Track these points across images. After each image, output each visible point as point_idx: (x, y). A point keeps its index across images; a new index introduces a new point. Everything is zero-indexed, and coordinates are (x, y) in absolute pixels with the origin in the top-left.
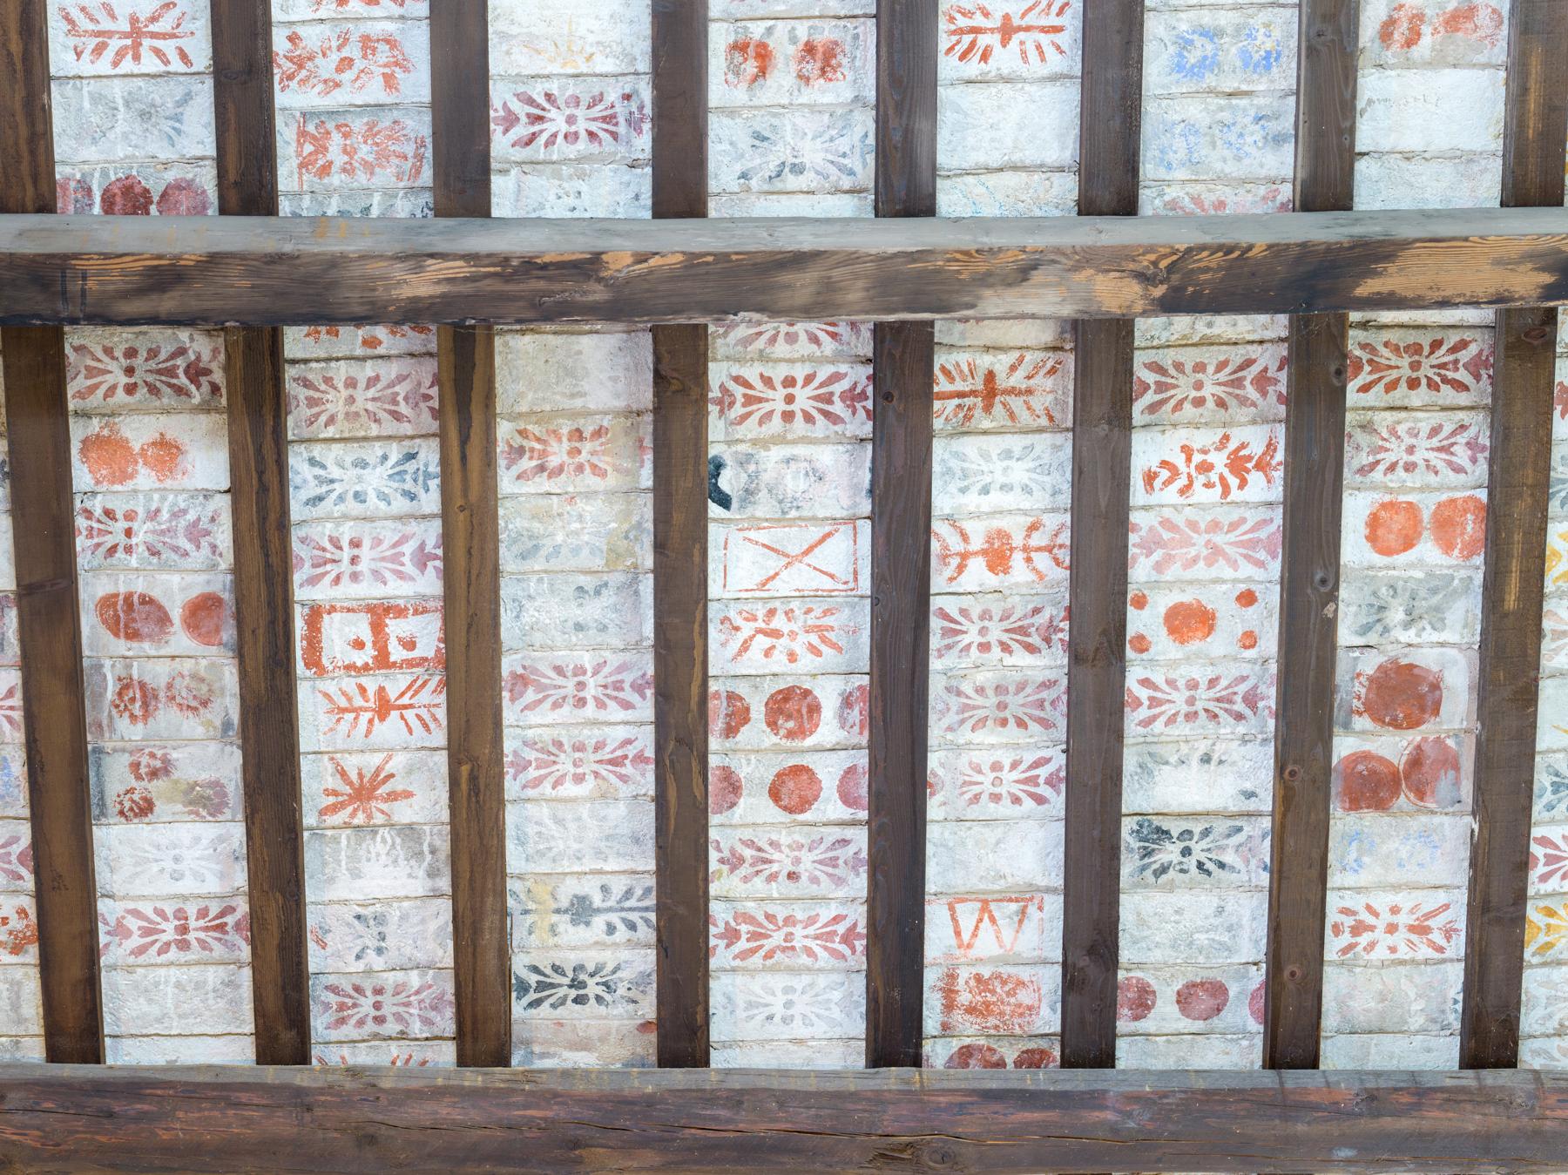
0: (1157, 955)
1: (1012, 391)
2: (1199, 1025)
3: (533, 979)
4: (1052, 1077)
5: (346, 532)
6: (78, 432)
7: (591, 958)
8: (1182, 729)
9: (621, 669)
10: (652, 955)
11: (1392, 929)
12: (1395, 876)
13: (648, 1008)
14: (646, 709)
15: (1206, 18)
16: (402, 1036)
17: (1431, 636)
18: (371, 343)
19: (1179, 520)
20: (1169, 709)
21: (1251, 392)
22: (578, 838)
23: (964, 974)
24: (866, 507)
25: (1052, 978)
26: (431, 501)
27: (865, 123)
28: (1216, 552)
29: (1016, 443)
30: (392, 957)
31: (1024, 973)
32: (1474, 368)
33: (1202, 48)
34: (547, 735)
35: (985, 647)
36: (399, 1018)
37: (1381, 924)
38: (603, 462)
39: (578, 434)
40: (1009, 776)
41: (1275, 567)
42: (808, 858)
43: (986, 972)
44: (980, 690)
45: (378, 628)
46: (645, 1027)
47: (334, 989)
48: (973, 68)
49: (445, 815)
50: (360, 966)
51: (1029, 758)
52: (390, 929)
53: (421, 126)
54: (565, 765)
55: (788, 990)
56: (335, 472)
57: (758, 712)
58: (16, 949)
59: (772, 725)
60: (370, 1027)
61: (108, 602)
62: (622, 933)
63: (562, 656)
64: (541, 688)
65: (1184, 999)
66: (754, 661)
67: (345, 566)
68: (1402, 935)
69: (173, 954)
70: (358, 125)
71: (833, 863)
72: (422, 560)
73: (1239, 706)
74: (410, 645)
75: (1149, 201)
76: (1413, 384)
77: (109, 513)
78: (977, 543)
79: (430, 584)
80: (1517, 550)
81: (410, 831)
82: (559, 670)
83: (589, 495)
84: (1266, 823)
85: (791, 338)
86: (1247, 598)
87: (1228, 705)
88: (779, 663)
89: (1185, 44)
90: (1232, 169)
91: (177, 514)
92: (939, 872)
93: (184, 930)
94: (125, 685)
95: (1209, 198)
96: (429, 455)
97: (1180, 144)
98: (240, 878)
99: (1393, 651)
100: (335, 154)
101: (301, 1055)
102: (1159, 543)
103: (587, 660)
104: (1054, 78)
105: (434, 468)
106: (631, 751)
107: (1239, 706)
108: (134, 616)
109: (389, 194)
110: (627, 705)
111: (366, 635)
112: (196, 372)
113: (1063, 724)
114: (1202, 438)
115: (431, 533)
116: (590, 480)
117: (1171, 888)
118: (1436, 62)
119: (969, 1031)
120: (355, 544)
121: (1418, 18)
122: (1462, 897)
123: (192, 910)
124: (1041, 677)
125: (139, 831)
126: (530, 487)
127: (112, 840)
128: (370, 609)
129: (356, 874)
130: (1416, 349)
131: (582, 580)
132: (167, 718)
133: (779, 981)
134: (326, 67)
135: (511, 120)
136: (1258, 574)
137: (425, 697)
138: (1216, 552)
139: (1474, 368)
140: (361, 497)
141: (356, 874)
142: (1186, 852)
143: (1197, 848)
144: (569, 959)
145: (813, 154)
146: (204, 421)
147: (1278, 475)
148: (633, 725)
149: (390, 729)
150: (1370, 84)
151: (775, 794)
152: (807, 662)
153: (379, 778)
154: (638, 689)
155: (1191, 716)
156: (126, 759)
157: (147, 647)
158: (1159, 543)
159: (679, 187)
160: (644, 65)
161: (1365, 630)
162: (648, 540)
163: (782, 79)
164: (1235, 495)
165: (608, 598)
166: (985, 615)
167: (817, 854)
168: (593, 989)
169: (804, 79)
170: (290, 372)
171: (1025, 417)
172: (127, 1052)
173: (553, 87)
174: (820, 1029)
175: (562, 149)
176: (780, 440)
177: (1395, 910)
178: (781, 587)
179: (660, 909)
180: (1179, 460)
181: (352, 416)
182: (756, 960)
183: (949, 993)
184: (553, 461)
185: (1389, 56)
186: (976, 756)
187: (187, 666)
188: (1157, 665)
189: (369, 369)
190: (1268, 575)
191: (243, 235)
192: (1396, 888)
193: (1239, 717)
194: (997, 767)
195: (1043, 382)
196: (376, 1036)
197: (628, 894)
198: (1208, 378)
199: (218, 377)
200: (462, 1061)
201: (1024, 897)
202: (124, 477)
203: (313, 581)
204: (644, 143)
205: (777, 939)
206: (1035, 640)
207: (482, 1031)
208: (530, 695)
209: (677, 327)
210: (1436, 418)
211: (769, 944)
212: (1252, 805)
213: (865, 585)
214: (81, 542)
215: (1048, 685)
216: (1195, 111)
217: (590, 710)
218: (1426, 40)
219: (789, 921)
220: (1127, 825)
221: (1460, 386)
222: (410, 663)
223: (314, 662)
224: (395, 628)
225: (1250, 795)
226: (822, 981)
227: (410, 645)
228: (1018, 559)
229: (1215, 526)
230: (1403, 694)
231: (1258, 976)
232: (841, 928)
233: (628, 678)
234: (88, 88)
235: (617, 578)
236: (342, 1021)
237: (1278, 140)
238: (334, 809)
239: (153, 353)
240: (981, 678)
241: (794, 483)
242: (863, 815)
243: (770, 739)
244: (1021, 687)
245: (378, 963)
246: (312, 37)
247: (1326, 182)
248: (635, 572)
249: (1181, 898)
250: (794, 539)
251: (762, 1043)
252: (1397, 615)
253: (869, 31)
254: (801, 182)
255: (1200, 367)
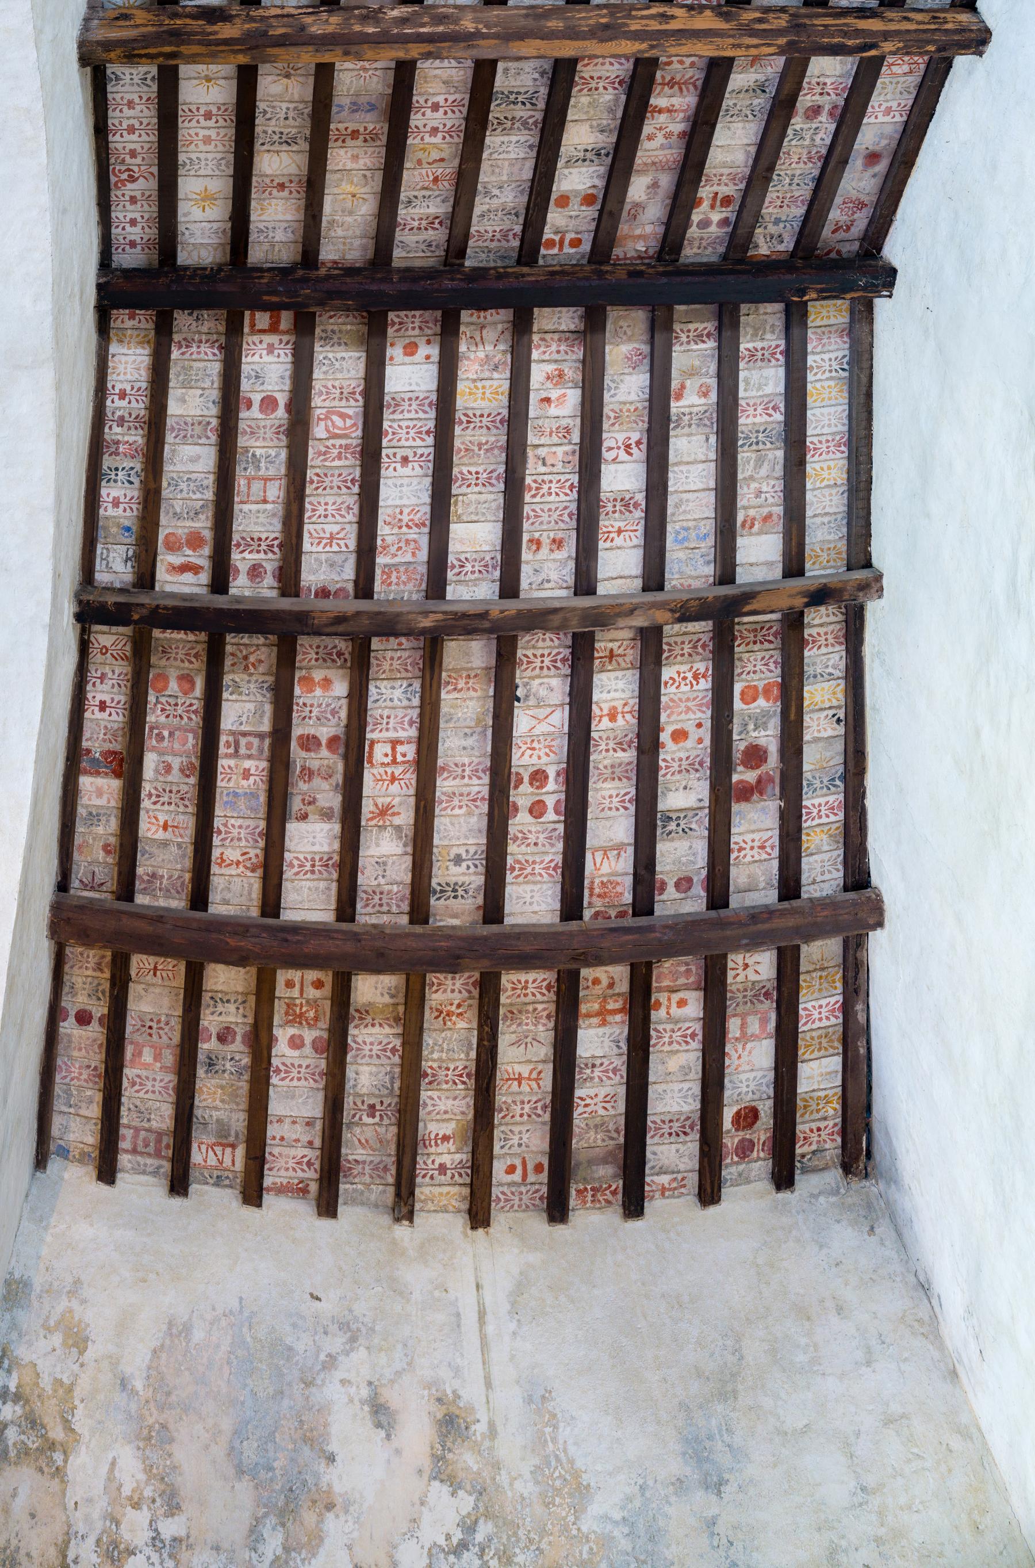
0: (668, 868)
1: (619, 655)
2: (683, 895)
3: (439, 888)
4: (630, 921)
5: (386, 713)
6: (298, 674)
7: (461, 879)
8: (677, 777)
9: (479, 764)
10: (483, 878)
11: (752, 848)
12: (753, 827)
13: (480, 900)
14: (486, 780)
15: (685, 524)
16: (389, 912)
17: (763, 733)
18: (400, 644)
19: (676, 698)
20: (672, 770)
21: (700, 650)
22: (459, 829)
23: (597, 881)
24: (567, 700)
25: (629, 880)
26: (416, 701)
27: (572, 564)
28: (688, 709)
29: (620, 674)
30: (388, 879)
31: (619, 879)
32: (775, 635)
33: (683, 534)
34: (450, 790)
35: (607, 751)
36: (388, 904)
37: (748, 847)
38: (477, 687)
39: (468, 677)
40: (615, 800)
41: (709, 713)
42: (542, 836)
43: (605, 880)
44: (606, 767)
45: (394, 749)
46: (479, 908)
47: (365, 892)
48: (608, 544)
49: (412, 822)
50: (376, 883)
51: (622, 792)
52: (388, 868)
53: (423, 569)
54: (456, 802)
55: (532, 891)
56: (384, 691)
57: (526, 779)
58: (253, 871)
59: (531, 784)
60: (377, 908)
61: (301, 737)
62: (472, 869)
63: (458, 760)
64: (449, 772)
65: (677, 885)
66: (526, 760)
67: (384, 726)
68: (756, 850)
69: (309, 875)
70: (402, 569)
71: (550, 838)
72: (411, 723)
73: (697, 766)
74: (404, 755)
75: (667, 586)
76: (755, 643)
77: (305, 704)
78: (606, 712)
79: (413, 732)
80: (794, 698)
81: (398, 828)
82: (456, 765)
83: (471, 699)
84: (707, 811)
85: (544, 640)
86: (699, 725)
87: (693, 766)
88: (535, 760)
89: (678, 533)
90: (693, 573)
91: (328, 705)
92: (591, 840)
93: (313, 866)
94: (303, 768)
95: (686, 584)
96: (417, 685)
97: (676, 566)
98: (336, 845)
99: (750, 740)
100: (394, 579)
101: (352, 919)
102: (669, 707)
103: (466, 761)
104: (635, 547)
105: (418, 689)
106: (480, 796)
107: (697, 766)
108: (310, 743)
109: (411, 593)
110: (479, 778)
111: (389, 752)
112: (340, 654)
113: (635, 778)
114: (684, 668)
115: (415, 713)
116: (472, 693)
117: (672, 840)
118: (760, 533)
119: (599, 904)
120: (388, 717)
121: (754, 519)
122: (777, 832)
123: (317, 858)
124: (627, 761)
125: (302, 826)
126: (451, 696)
127: (293, 828)
128: (392, 742)
129: (378, 845)
130: (756, 630)
131: (467, 730)
132: (317, 781)
133: (529, 887)
134: (393, 550)
135: (453, 567)
136: (703, 716)
137: (408, 775)
138: (688, 709)
139: (775, 635)
140: (393, 700)
141: (378, 845)
142: (678, 825)
143: (682, 823)
144: (452, 880)
145: (554, 576)
146: (341, 672)
147: (710, 679)
148: (480, 786)
149: (395, 788)
150: (740, 542)
151: (531, 812)
152: (545, 759)
153: (389, 807)
154: (484, 771)
155: (680, 772)
156: (300, 797)
157: (313, 755)
158: (669, 707)
159: (509, 588)
160: (499, 548)
161: (740, 733)
162: (491, 715)
163: (544, 551)
164: (695, 687)
165: (475, 737)
166: (608, 738)
167: (545, 835)
168: (460, 892)
169: (552, 550)
170: (372, 654)
171: (623, 664)
172: (288, 916)
173: (468, 556)
174: (544, 907)
175: (470, 576)
176: (539, 677)
177: (753, 841)
178: (536, 731)
179: (487, 859)
180: (676, 676)
181: (391, 671)
182: (521, 879)
183: (591, 889)
184: (459, 687)
185: (744, 532)
186: (604, 793)
187: (326, 762)
188: (670, 752)
189: (399, 654)
190: (706, 716)
191: (363, 605)
192: (753, 832)
193: (697, 770)
194: (611, 797)
195: (630, 652)
196: (379, 912)
197: (476, 853)
198: (686, 646)
199: (347, 656)
200: (411, 922)
201: (620, 847)
202: (312, 691)
203: (373, 731)
204: (497, 574)
205: (529, 870)
206: (625, 746)
207: (419, 912)
208: (445, 775)
209: (504, 635)
210: (763, 654)
211: (525, 872)
212: (701, 804)
213: (566, 729)
214: (294, 714)
215: (629, 764)
216: (681, 555)
217: (466, 780)
218: (756, 526)
219: (534, 862)
220: (659, 816)
221: (770, 642)
222: (404, 762)
223: (370, 762)
224: (400, 749)
225: (701, 800)
226: (545, 886)
227: (404, 755)
228: (620, 716)
229: (688, 700)
230: (755, 755)
231: (704, 873)
232: (553, 865)
233: (481, 767)
234: (314, 556)
235: (479, 729)
236: (367, 905)
237: (709, 563)
238: (372, 819)
239: (326, 647)
240: (606, 762)
241: (543, 692)
242: (562, 818)
243: (531, 790)
244: (620, 765)
245: (382, 881)
246: (389, 540)
247: (726, 574)
248: (485, 727)
249: (677, 844)
250: (542, 713)
251: (522, 913)
252: (751, 727)
253: (574, 534)
254: (549, 585)
255: (683, 643)
